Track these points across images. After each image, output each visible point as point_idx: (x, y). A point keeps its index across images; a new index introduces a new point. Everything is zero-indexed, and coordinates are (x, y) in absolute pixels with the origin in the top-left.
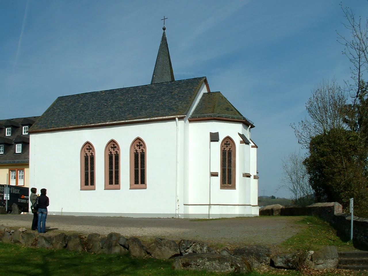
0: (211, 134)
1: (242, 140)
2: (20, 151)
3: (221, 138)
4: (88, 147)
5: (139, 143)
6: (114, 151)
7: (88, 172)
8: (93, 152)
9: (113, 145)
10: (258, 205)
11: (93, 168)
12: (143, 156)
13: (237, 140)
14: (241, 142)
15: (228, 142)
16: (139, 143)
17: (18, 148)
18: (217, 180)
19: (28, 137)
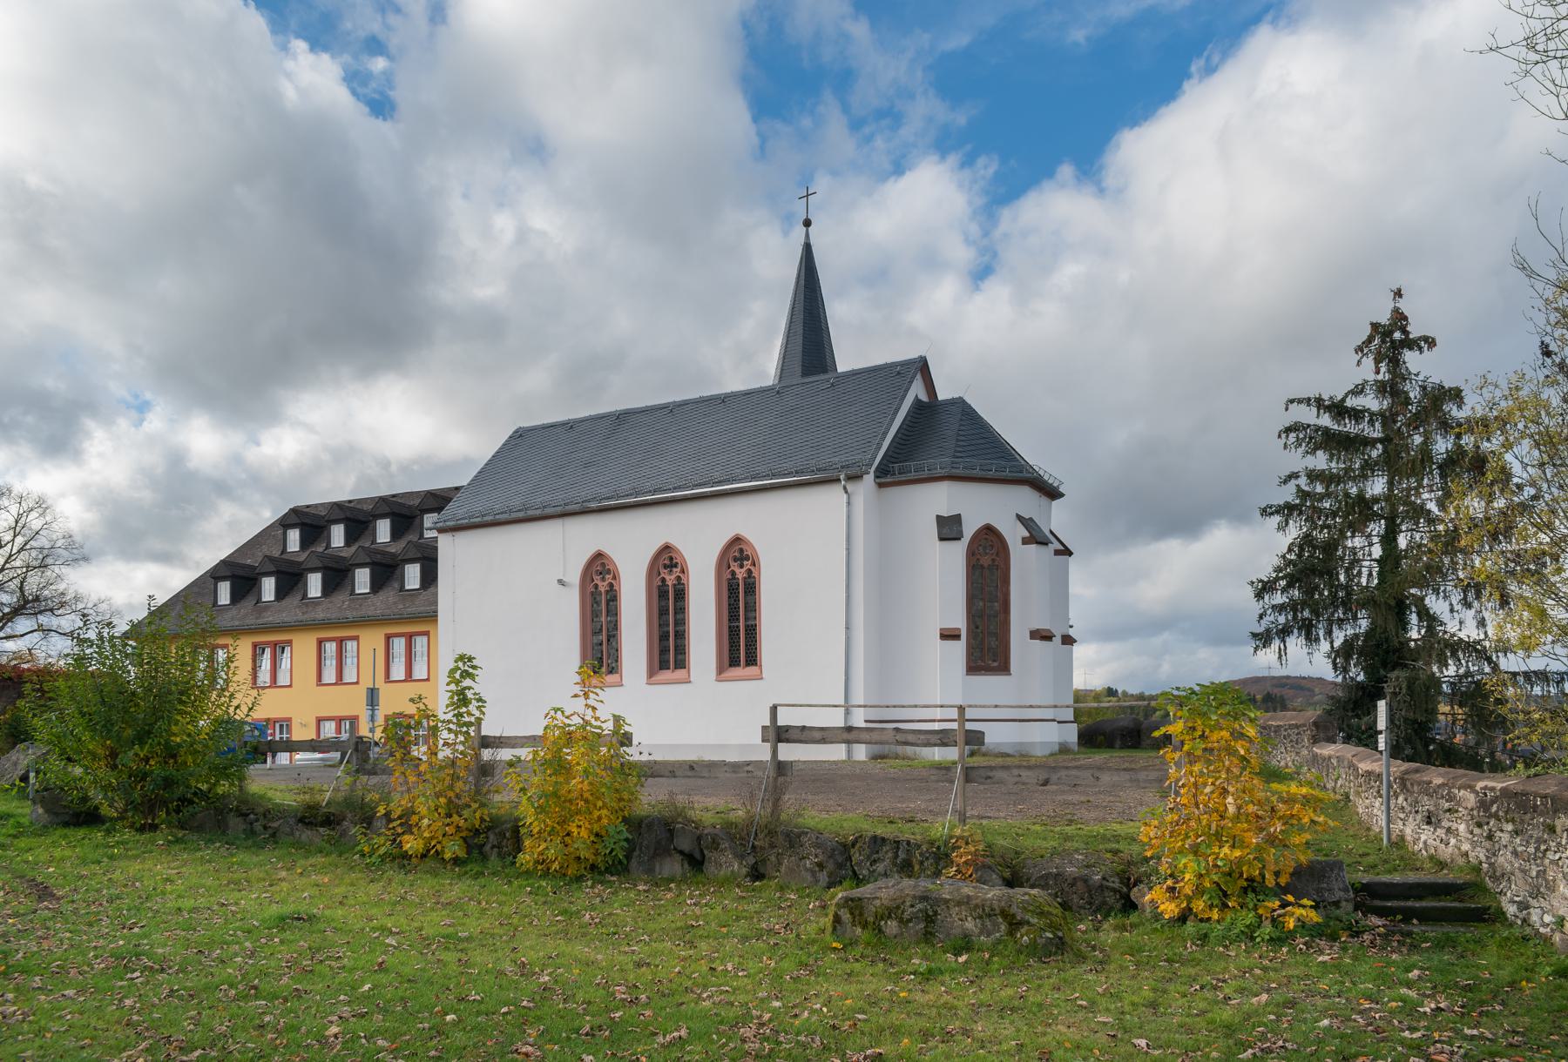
0: (941, 521)
1: (1027, 534)
2: (365, 588)
3: (969, 529)
4: (599, 569)
5: (737, 554)
6: (605, 584)
7: (738, 627)
8: (754, 565)
9: (667, 561)
10: (1075, 717)
11: (681, 622)
12: (751, 587)
13: (1013, 534)
14: (1025, 541)
15: (989, 538)
16: (737, 554)
17: (412, 575)
18: (959, 649)
19: (433, 544)
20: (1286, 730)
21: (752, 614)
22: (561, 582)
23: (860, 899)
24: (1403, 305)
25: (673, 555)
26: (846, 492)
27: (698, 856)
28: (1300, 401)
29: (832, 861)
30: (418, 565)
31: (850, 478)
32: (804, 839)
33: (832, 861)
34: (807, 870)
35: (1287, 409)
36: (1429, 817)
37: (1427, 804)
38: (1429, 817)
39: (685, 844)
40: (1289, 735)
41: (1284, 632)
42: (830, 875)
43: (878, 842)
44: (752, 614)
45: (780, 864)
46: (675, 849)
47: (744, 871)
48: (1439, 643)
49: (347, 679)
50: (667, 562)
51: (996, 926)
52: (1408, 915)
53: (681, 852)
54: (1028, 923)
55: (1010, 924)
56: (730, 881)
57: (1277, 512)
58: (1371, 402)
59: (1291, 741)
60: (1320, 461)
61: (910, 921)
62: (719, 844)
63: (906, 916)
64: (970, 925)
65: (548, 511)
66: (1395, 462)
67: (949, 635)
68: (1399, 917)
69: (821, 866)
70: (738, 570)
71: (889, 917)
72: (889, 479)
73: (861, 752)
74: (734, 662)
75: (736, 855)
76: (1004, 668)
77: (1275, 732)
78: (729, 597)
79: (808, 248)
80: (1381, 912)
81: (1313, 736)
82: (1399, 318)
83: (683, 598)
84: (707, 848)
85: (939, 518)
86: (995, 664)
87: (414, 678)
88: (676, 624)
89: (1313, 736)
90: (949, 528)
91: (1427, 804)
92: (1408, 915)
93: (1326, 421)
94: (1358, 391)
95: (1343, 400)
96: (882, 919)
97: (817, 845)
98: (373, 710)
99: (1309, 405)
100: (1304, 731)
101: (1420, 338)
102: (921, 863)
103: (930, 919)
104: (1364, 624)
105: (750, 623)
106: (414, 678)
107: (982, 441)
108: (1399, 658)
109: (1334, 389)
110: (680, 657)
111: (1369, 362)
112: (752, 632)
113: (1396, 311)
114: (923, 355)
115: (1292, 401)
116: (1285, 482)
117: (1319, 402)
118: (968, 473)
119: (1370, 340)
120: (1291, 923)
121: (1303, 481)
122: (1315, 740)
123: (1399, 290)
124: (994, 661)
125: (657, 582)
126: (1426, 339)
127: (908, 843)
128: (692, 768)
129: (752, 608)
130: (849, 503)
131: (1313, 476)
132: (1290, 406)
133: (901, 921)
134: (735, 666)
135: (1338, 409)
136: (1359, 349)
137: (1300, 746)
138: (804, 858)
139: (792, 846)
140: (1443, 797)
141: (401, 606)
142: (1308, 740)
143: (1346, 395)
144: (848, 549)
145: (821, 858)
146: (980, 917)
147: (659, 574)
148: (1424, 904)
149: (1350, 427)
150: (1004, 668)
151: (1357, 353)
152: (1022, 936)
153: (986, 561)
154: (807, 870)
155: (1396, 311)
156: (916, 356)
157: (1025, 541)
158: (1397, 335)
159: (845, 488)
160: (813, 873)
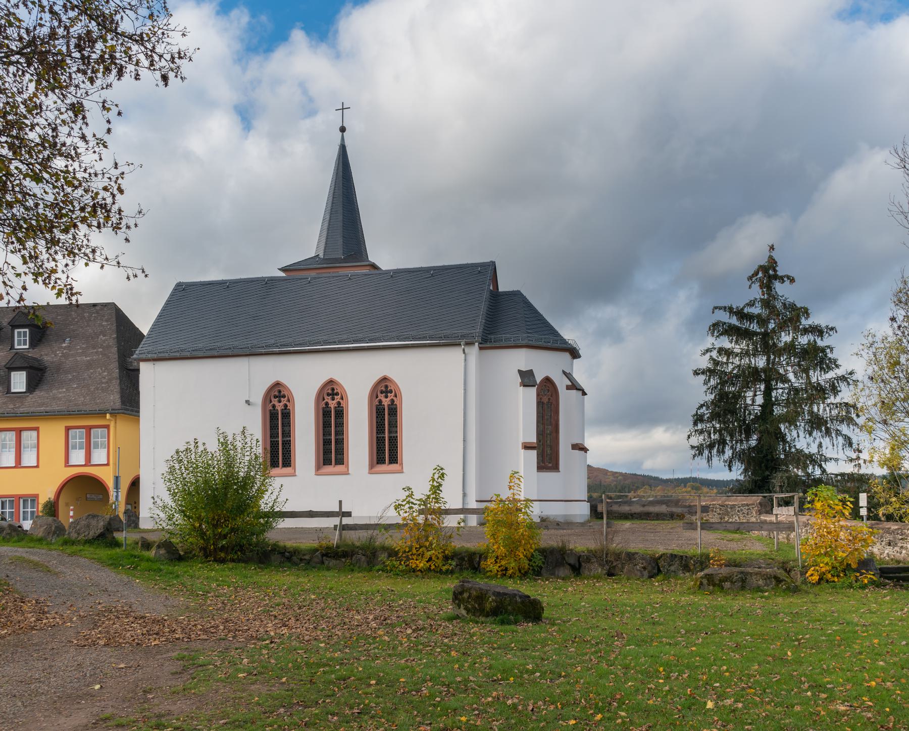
12: (394, 411)
13: (561, 383)
14: (568, 388)
20: (739, 507)
21: (394, 429)
22: (248, 402)
23: (712, 574)
24: (775, 255)
25: (335, 387)
26: (464, 353)
27: (577, 566)
28: (720, 308)
29: (650, 566)
30: (25, 373)
31: (467, 344)
32: (636, 556)
33: (650, 566)
34: (637, 570)
35: (713, 313)
36: (890, 543)
37: (889, 537)
38: (890, 543)
39: (572, 561)
40: (742, 510)
41: (711, 447)
42: (649, 572)
43: (673, 556)
44: (394, 429)
45: (623, 568)
46: (566, 563)
47: (605, 572)
48: (803, 456)
49: (25, 462)
50: (330, 391)
51: (771, 582)
52: (899, 579)
53: (570, 565)
54: (785, 581)
55: (777, 581)
56: (598, 578)
57: (703, 373)
58: (756, 310)
59: (744, 513)
60: (725, 343)
61: (735, 582)
62: (590, 560)
63: (734, 580)
64: (761, 582)
65: (236, 352)
66: (767, 345)
67: (527, 447)
68: (895, 580)
69: (644, 568)
70: (384, 400)
71: (727, 581)
72: (488, 345)
73: (473, 521)
74: (380, 460)
75: (600, 565)
76: (555, 467)
77: (731, 508)
78: (377, 417)
79: (343, 149)
80: (889, 578)
81: (759, 511)
82: (772, 263)
83: (342, 417)
84: (583, 562)
85: (520, 371)
86: (550, 465)
87: (93, 463)
88: (337, 434)
89: (759, 511)
90: (527, 378)
91: (889, 537)
92: (899, 579)
93: (734, 321)
94: (751, 304)
95: (742, 309)
96: (723, 582)
97: (643, 559)
98: (117, 492)
99: (725, 311)
100: (753, 508)
101: (785, 276)
102: (694, 565)
103: (743, 581)
104: (753, 442)
105: (392, 435)
106: (93, 463)
107: (539, 322)
108: (775, 464)
109: (738, 303)
110: (339, 456)
111: (756, 286)
112: (394, 443)
113: (771, 257)
114: (493, 260)
115: (716, 308)
116: (704, 354)
117: (730, 310)
118: (545, 345)
119: (756, 273)
120: (866, 581)
121: (714, 354)
122: (760, 513)
123: (773, 245)
124: (550, 463)
125: (323, 405)
126: (788, 277)
127: (686, 557)
128: (558, 524)
129: (394, 425)
130: (465, 360)
131: (721, 351)
132: (715, 311)
133: (732, 582)
134: (381, 463)
135: (741, 315)
136: (750, 278)
137: (749, 516)
138: (636, 565)
139: (630, 560)
140: (898, 534)
141: (11, 406)
142: (756, 513)
143: (745, 307)
144: (465, 390)
145: (645, 564)
146: (765, 579)
147: (324, 399)
148: (901, 575)
149: (746, 325)
150: (555, 467)
151: (748, 280)
152: (782, 586)
153: (545, 400)
154: (637, 570)
155: (771, 257)
156: (489, 261)
157: (568, 388)
158: (771, 272)
159: (464, 350)
160: (641, 572)
